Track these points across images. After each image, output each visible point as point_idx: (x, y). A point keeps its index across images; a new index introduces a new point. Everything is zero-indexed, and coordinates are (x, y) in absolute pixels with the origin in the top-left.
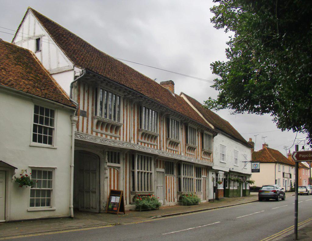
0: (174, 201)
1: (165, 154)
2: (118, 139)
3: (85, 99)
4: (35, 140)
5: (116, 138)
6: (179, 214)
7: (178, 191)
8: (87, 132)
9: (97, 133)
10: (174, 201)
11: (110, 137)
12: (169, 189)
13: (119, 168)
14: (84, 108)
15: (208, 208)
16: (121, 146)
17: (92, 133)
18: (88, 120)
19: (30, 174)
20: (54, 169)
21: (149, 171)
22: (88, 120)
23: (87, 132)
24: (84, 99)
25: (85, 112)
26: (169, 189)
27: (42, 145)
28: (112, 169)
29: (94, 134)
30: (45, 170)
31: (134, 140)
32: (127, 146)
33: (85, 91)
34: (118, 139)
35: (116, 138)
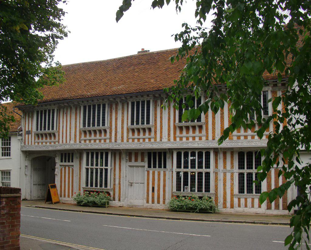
0: (164, 203)
1: (89, 146)
2: (57, 143)
3: (30, 122)
4: (3, 156)
5: (55, 143)
6: (179, 219)
7: (175, 190)
8: (31, 144)
9: (38, 143)
10: (164, 203)
11: (244, 138)
12: (153, 188)
13: (73, 166)
14: (28, 129)
15: (234, 220)
16: (59, 148)
17: (35, 144)
18: (32, 136)
19: (56, 174)
20: (10, 170)
21: (204, 170)
22: (32, 136)
23: (31, 144)
24: (29, 123)
25: (30, 131)
26: (153, 188)
27: (6, 157)
28: (67, 168)
29: (36, 144)
30: (7, 171)
31: (75, 141)
32: (66, 147)
33: (65, 113)
34: (57, 143)
35: (55, 143)
